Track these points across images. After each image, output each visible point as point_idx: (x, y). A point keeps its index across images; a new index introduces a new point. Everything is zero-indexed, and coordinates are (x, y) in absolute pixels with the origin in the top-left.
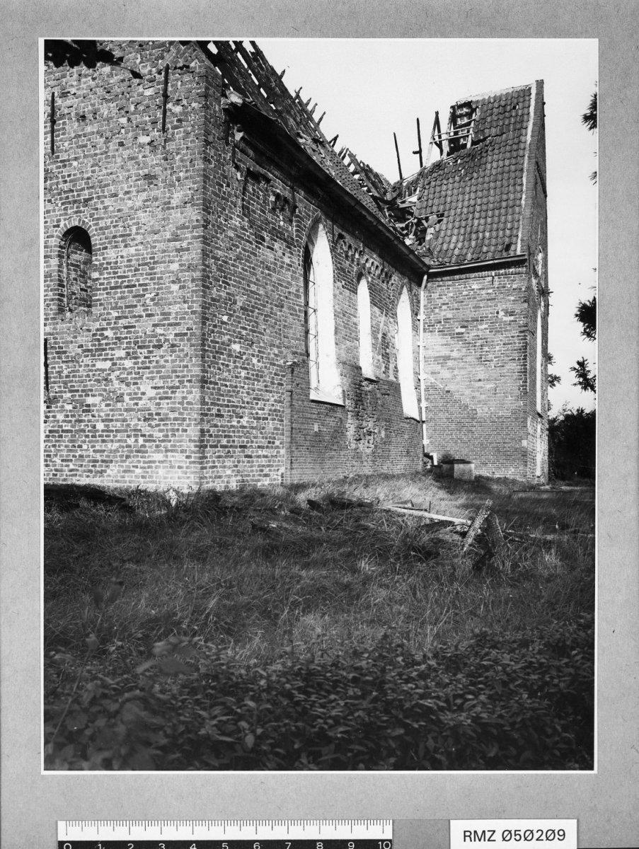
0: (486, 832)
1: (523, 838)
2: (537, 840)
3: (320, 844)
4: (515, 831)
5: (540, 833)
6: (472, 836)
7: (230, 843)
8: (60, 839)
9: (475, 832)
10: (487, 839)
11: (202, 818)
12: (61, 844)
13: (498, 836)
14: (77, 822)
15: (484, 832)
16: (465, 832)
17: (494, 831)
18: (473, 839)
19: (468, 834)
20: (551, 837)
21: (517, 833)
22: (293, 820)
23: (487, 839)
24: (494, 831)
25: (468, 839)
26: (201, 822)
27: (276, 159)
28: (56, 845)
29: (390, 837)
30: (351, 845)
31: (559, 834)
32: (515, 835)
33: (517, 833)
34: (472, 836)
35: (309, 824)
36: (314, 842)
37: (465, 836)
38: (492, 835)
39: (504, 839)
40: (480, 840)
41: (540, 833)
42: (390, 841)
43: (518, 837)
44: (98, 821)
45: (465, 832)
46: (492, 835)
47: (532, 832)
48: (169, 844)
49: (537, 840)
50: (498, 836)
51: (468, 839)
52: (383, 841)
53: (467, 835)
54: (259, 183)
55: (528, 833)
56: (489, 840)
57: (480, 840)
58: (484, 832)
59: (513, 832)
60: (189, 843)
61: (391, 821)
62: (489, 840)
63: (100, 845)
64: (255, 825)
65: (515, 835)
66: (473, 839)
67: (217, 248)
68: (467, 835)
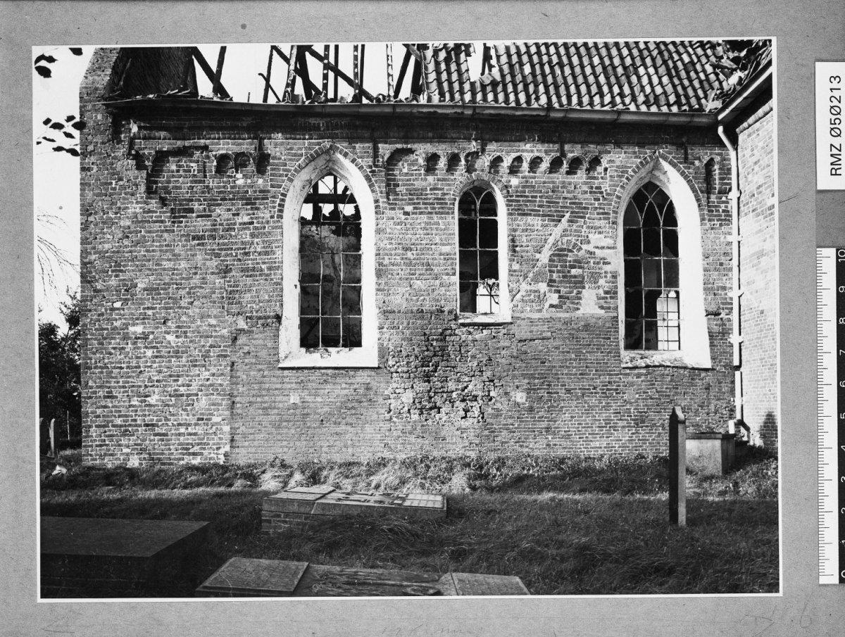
0: (833, 153)
1: (838, 116)
2: (840, 102)
3: (841, 321)
4: (831, 124)
5: (833, 99)
6: (836, 167)
7: (840, 411)
8: (837, 581)
9: (832, 164)
10: (838, 153)
11: (816, 394)
12: (842, 580)
13: (836, 142)
14: (818, 326)
15: (832, 155)
16: (832, 175)
17: (831, 145)
18: (839, 167)
19: (834, 172)
20: (838, 131)
21: (833, 122)
22: (816, 378)
23: (838, 153)
24: (831, 145)
25: (838, 172)
26: (818, 268)
27: (214, 124)
28: (842, 586)
29: (834, 250)
30: (841, 289)
31: (836, 119)
32: (835, 124)
33: (833, 122)
34: (836, 167)
35: (822, 491)
36: (839, 326)
37: (836, 174)
38: (837, 148)
39: (839, 135)
40: (840, 160)
41: (833, 99)
42: (837, 250)
43: (837, 121)
44: (817, 308)
45: (832, 175)
46: (837, 148)
47: (832, 107)
48: (840, 313)
49: (840, 102)
50: (836, 142)
51: (838, 172)
52: (838, 257)
53: (835, 173)
54: (191, 155)
55: (833, 111)
56: (840, 151)
57: (840, 160)
58: (832, 155)
59: (833, 126)
60: (840, 450)
61: (818, 249)
62: (840, 151)
63: (843, 541)
64: (824, 561)
65: (835, 124)
66: (839, 167)
67: (133, 271)
68: (835, 173)
